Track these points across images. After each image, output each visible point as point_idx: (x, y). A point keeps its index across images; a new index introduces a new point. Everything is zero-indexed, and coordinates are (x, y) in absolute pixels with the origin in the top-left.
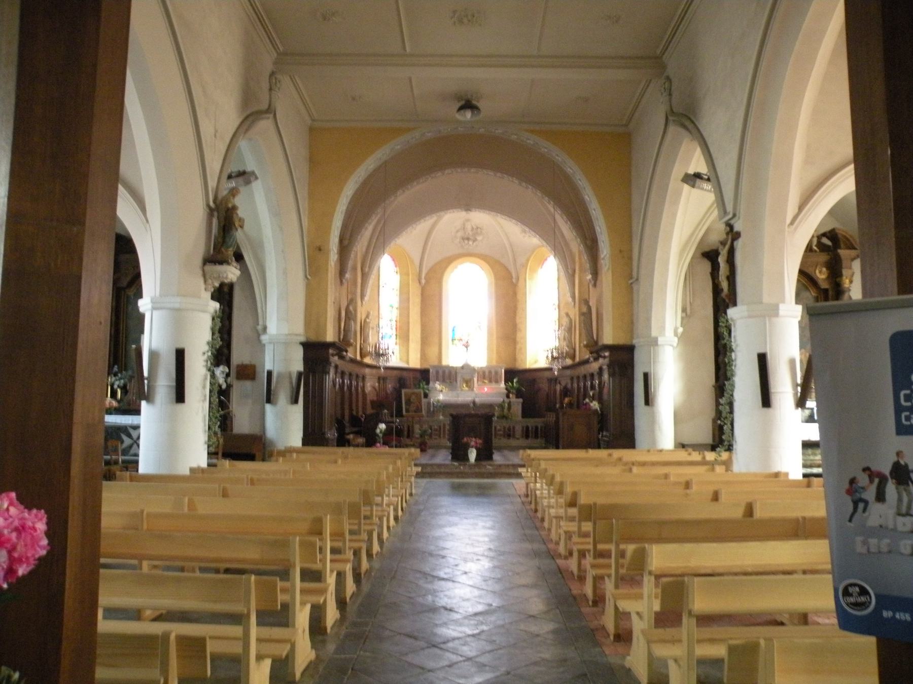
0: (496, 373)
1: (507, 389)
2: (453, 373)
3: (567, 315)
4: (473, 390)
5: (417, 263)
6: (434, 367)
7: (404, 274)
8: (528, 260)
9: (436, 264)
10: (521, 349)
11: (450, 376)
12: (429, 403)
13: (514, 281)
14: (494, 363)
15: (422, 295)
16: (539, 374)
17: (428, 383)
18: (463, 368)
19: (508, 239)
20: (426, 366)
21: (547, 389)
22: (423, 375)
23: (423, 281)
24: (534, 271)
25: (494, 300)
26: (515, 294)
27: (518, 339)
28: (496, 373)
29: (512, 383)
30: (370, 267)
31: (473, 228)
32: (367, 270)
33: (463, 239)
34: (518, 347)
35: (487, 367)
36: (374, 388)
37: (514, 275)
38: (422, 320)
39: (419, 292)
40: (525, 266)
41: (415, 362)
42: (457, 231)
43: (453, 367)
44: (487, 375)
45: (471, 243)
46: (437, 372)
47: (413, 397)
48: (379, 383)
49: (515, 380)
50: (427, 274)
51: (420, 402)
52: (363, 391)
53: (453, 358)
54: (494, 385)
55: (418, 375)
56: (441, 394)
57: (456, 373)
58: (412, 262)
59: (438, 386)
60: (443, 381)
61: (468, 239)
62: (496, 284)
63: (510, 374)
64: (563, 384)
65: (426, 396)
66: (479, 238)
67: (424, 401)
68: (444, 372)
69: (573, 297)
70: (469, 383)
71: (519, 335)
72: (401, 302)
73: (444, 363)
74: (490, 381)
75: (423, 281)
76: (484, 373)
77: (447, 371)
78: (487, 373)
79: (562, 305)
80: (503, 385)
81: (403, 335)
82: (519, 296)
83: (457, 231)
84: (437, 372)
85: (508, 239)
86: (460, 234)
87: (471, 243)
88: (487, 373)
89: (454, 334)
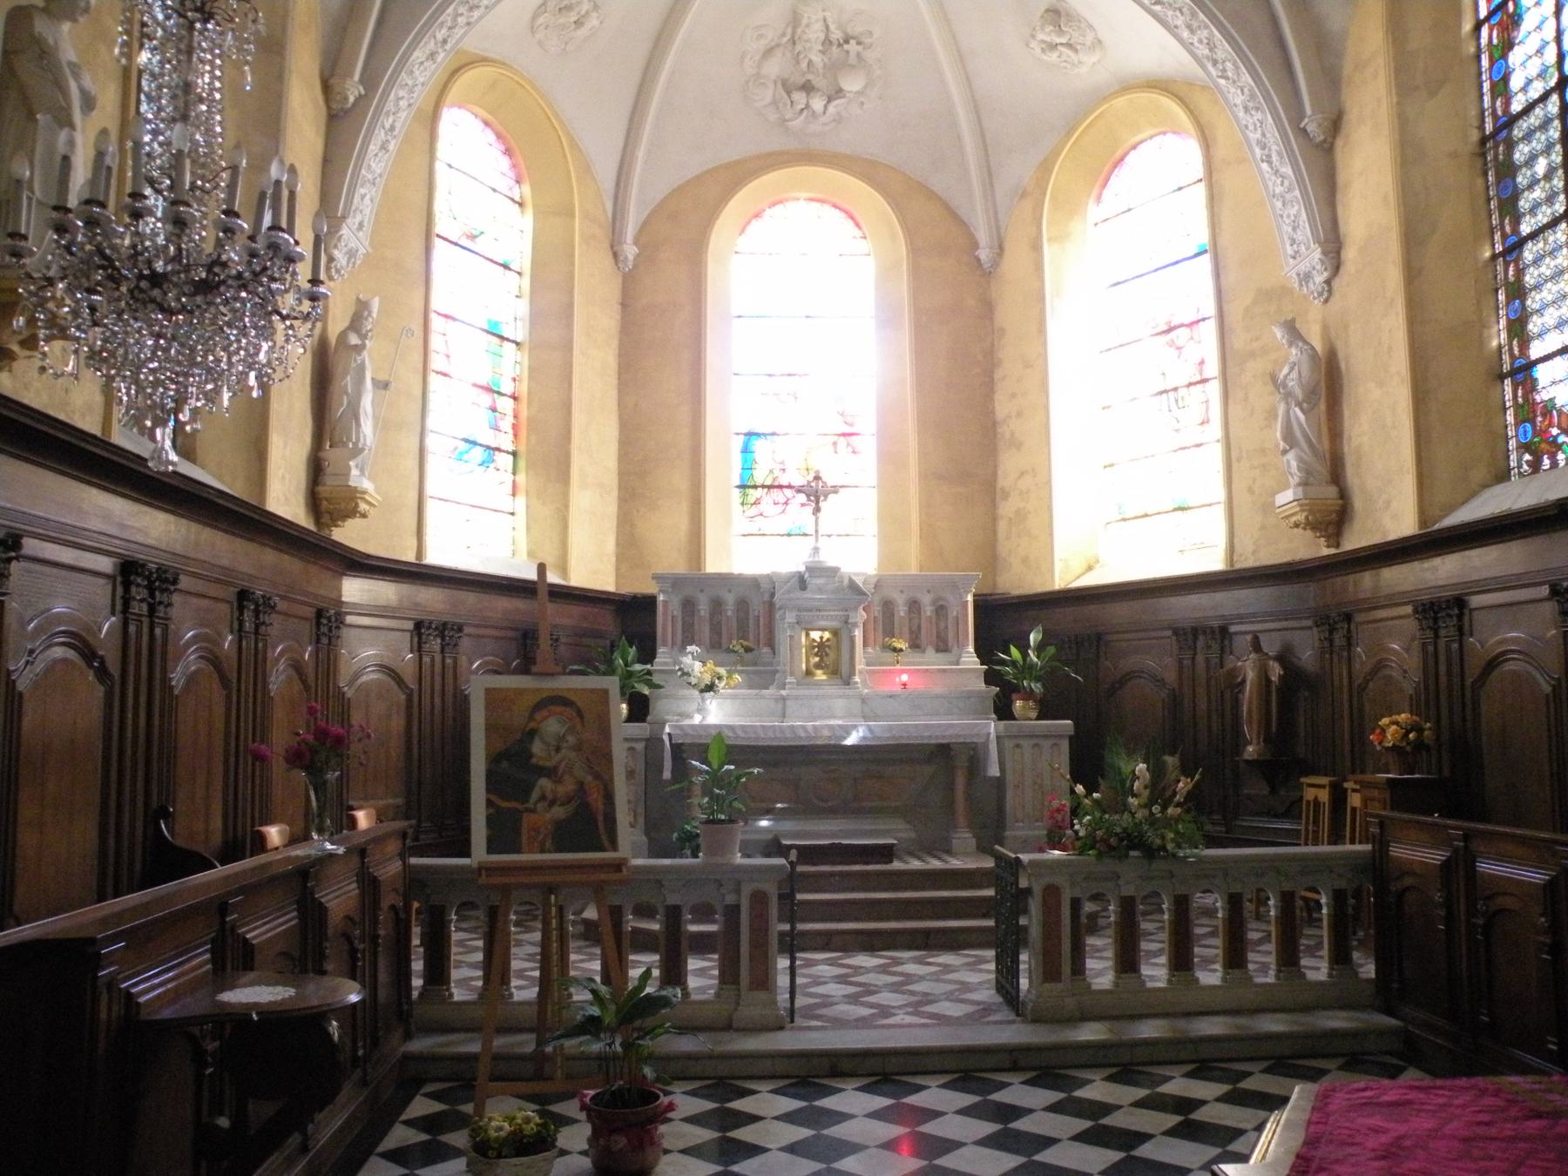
0: (941, 610)
1: (990, 678)
2: (757, 607)
3: (1294, 332)
4: (847, 682)
5: (608, 185)
6: (676, 582)
7: (552, 214)
8: (1046, 167)
9: (679, 191)
10: (1021, 515)
11: (743, 622)
12: (653, 743)
13: (984, 254)
14: (914, 570)
15: (626, 304)
16: (1120, 612)
17: (648, 655)
18: (801, 581)
19: (968, 81)
20: (643, 586)
21: (1413, 662)
22: (627, 623)
23: (630, 251)
24: (1071, 207)
25: (904, 338)
26: (987, 308)
27: (1002, 482)
28: (941, 610)
29: (1024, 648)
30: (370, 81)
31: (827, 42)
32: (353, 90)
33: (788, 88)
34: (1006, 509)
35: (879, 584)
36: (213, 659)
37: (983, 236)
38: (621, 404)
39: (610, 289)
40: (1033, 193)
41: (592, 566)
42: (768, 52)
43: (754, 583)
44: (902, 618)
45: (818, 104)
46: (689, 605)
47: (552, 726)
48: (419, 649)
49: (1034, 638)
50: (644, 226)
51: (599, 757)
52: (165, 680)
53: (748, 545)
54: (932, 660)
55: (607, 621)
56: (712, 705)
57: (771, 605)
58: (586, 169)
59: (695, 664)
60: (716, 646)
61: (808, 88)
62: (916, 272)
63: (999, 619)
64: (1271, 646)
65: (640, 709)
66: (852, 84)
67: (623, 731)
68: (717, 605)
69: (1333, 246)
70: (833, 661)
71: (1010, 465)
72: (536, 318)
73: (714, 564)
74: (915, 645)
75: (630, 251)
76: (888, 606)
77: (730, 599)
78: (901, 611)
79: (1235, 311)
80: (970, 659)
81: (544, 454)
82: (1008, 314)
83: (768, 52)
84: (689, 605)
85: (968, 81)
86: (774, 68)
87: (818, 104)
88: (901, 611)
89: (748, 468)
